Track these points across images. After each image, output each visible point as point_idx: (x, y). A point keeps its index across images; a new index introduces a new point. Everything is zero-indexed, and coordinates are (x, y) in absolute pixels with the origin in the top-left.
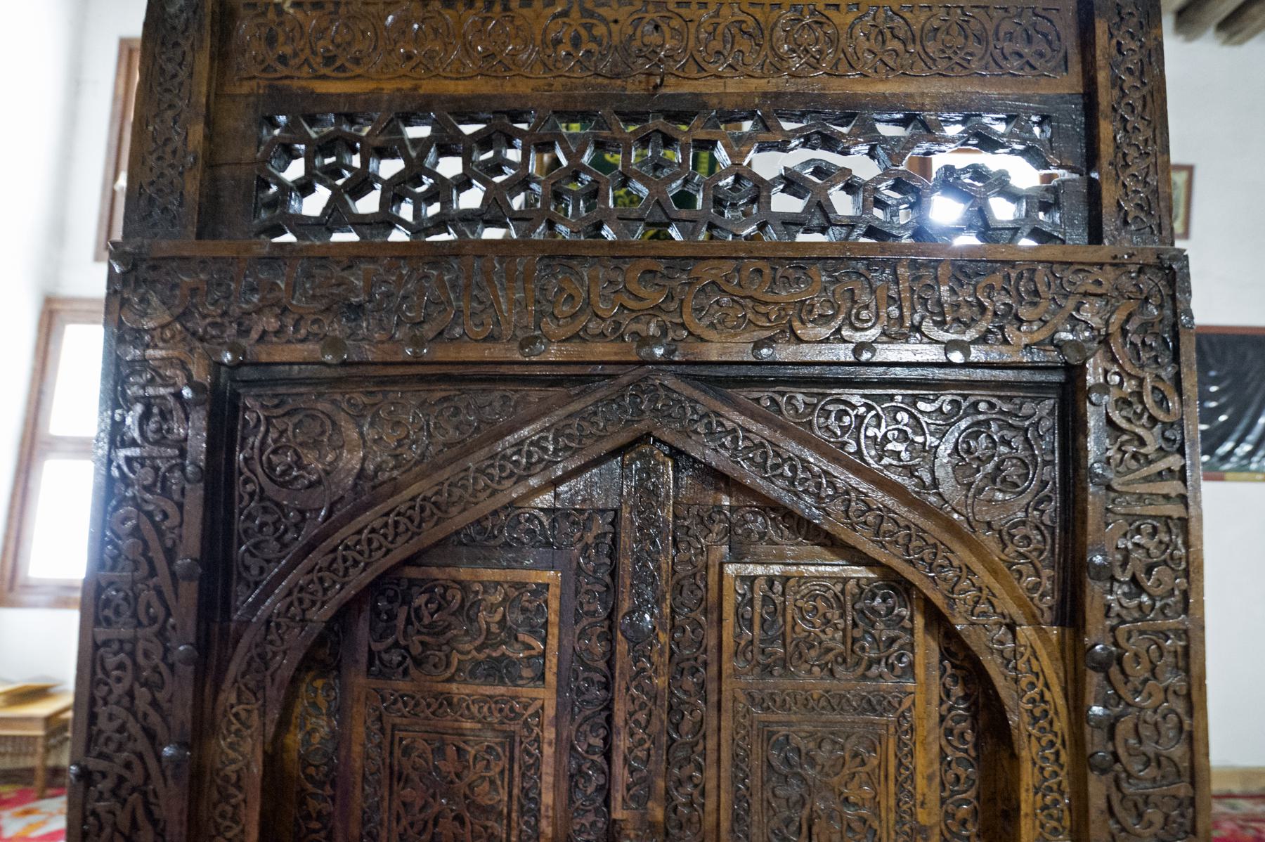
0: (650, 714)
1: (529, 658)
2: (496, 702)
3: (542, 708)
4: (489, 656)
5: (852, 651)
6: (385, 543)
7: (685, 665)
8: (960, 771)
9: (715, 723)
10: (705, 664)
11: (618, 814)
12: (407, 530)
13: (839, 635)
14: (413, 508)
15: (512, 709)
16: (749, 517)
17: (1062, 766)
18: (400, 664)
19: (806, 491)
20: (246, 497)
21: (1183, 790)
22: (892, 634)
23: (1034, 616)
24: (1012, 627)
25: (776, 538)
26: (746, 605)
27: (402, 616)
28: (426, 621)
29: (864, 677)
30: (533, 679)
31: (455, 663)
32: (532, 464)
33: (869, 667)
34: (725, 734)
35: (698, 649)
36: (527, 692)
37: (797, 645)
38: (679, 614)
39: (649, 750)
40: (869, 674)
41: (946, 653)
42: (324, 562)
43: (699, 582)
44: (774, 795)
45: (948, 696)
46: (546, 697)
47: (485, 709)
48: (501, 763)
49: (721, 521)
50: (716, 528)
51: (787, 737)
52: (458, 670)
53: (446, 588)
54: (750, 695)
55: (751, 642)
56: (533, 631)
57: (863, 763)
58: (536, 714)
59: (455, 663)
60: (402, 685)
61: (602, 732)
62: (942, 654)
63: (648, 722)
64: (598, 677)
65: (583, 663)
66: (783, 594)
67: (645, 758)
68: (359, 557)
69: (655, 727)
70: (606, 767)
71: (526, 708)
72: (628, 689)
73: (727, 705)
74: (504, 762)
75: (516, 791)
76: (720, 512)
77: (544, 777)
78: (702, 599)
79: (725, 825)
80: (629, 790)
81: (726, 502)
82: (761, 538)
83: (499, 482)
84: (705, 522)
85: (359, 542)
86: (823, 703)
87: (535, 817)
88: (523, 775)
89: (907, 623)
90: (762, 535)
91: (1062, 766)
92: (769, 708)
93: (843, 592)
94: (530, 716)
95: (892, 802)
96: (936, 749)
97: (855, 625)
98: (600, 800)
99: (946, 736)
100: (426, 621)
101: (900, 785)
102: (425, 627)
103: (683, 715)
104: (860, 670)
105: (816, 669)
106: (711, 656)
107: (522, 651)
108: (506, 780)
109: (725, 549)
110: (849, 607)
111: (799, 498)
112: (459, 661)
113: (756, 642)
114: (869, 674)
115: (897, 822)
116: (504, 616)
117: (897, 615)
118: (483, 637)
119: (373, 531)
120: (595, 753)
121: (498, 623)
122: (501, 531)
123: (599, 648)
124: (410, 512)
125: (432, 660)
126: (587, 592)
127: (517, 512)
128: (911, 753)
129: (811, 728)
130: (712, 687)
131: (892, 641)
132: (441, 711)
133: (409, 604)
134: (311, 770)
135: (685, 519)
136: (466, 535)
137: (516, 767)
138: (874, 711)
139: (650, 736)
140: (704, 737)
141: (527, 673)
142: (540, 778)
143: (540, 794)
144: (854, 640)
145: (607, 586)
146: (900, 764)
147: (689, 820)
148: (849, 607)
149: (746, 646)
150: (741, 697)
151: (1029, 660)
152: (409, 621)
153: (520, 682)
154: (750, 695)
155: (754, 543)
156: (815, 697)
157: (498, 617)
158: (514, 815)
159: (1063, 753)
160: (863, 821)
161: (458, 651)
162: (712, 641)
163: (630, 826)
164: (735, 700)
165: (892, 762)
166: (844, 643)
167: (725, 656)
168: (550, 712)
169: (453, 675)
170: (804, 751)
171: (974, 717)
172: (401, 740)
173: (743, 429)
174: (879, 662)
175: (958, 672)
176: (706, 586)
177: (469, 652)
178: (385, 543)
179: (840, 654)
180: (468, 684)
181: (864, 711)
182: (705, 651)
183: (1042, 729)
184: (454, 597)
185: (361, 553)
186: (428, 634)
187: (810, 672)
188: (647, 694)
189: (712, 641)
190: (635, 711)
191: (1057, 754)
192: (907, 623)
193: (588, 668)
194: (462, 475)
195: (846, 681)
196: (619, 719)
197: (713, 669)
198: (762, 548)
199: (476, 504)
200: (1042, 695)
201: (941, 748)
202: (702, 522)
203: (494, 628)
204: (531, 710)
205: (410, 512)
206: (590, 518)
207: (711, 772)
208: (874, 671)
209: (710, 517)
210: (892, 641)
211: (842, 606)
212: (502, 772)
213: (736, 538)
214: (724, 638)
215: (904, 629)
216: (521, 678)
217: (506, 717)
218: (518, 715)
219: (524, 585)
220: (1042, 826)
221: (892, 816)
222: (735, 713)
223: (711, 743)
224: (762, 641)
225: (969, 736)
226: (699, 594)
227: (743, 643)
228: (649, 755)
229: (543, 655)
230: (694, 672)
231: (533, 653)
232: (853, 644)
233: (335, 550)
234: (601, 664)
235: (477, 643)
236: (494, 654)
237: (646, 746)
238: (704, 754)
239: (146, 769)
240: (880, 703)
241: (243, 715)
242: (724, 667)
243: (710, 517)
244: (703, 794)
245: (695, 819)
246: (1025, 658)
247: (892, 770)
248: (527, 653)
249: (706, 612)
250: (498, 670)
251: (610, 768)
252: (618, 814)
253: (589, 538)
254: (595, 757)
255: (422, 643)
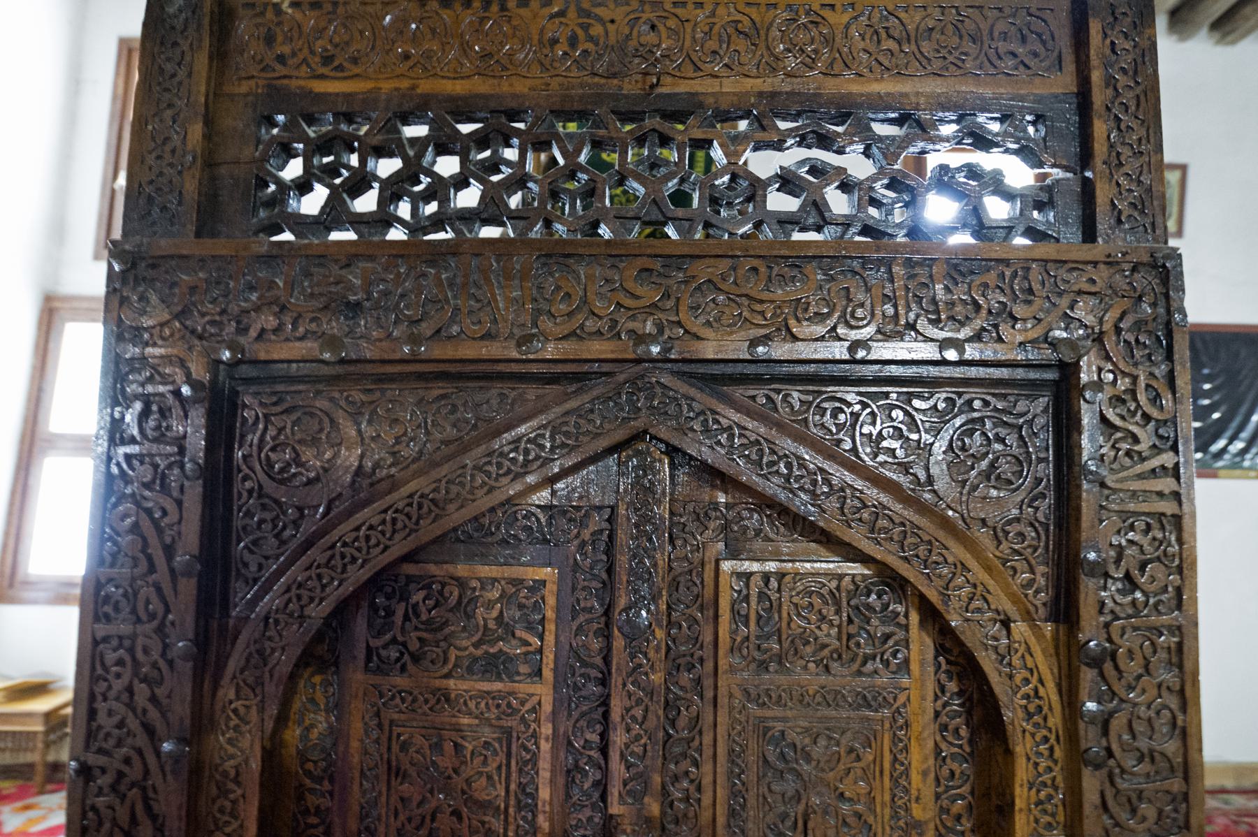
0: (646, 710)
1: (526, 654)
2: (493, 698)
3: (539, 703)
4: (486, 652)
5: (848, 647)
6: (382, 540)
7: (681, 661)
8: (955, 766)
9: (711, 718)
10: (701, 660)
11: (615, 809)
12: (405, 526)
13: (834, 631)
14: (410, 505)
15: (509, 705)
16: (745, 514)
17: (1056, 762)
18: (398, 660)
19: (801, 488)
20: (245, 494)
21: (1176, 785)
22: (887, 630)
23: (1028, 612)
24: (1006, 623)
25: (771, 535)
26: (742, 601)
27: (400, 613)
28: (424, 617)
29: (859, 673)
30: (530, 675)
31: (453, 659)
32: (529, 461)
33: (864, 663)
34: (721, 730)
35: (694, 645)
36: (524, 688)
37: (792, 642)
38: (675, 611)
39: (645, 746)
40: (864, 670)
41: (940, 649)
42: (322, 559)
43: (695, 579)
44: (770, 790)
45: (943, 692)
46: (543, 692)
47: (483, 705)
48: (498, 759)
49: (717, 518)
50: (712, 525)
51: (783, 733)
52: (456, 666)
53: (443, 585)
54: (746, 691)
55: (747, 638)
56: (530, 628)
57: (858, 759)
58: (534, 710)
59: (453, 659)
60: (400, 681)
61: (599, 728)
62: (937, 650)
63: (645, 717)
64: (594, 673)
65: (580, 659)
66: (779, 590)
67: (641, 754)
68: (357, 554)
69: (652, 722)
70: (602, 762)
71: (523, 703)
72: (624, 685)
73: (723, 700)
74: (502, 757)
75: (513, 787)
76: (716, 509)
77: (541, 772)
78: (698, 596)
79: (721, 820)
80: (625, 785)
81: (722, 499)
82: (757, 535)
83: (496, 480)
84: (701, 519)
85: (357, 539)
86: (819, 699)
87: (532, 812)
88: (520, 771)
89: (902, 620)
90: (758, 532)
91: (1056, 762)
92: (765, 704)
93: (838, 588)
94: (527, 712)
95: (887, 797)
96: (931, 744)
97: (850, 621)
98: (596, 795)
99: (941, 732)
100: (424, 617)
101: (895, 781)
102: (423, 623)
103: (679, 711)
104: (855, 666)
105: (812, 665)
106: (707, 652)
107: (519, 647)
108: (503, 775)
109: (721, 545)
110: (844, 603)
111: (795, 495)
112: (457, 657)
113: (752, 638)
114: (864, 670)
115: (892, 817)
116: (501, 612)
117: (892, 612)
118: (480, 633)
119: (371, 528)
120: (591, 749)
121: (495, 619)
122: (498, 528)
123: (596, 644)
124: (407, 509)
125: (430, 656)
126: (584, 589)
127: (514, 509)
128: (906, 749)
129: (806, 724)
130: (708, 682)
131: (887, 637)
132: (438, 707)
133: (407, 600)
134: (310, 766)
135: (681, 516)
136: (463, 532)
137: (513, 763)
138: (869, 706)
139: (646, 731)
140: (700, 733)
141: (524, 669)
142: (537, 773)
143: (537, 789)
144: (850, 637)
145: (604, 583)
146: (895, 759)
147: (685, 815)
148: (844, 603)
149: (742, 642)
150: (737, 693)
151: (1023, 656)
152: (406, 618)
153: (517, 678)
154: (746, 691)
155: (750, 540)
156: (811, 692)
157: (495, 613)
158: (511, 810)
159: (1057, 748)
160: (859, 816)
161: (455, 648)
162: (708, 638)
163: (626, 821)
164: (731, 696)
165: (888, 758)
166: (839, 639)
167: (721, 653)
168: (547, 707)
169: (451, 671)
170: (799, 747)
171: (969, 713)
172: (399, 735)
173: (739, 426)
174: (874, 658)
175: (953, 668)
176: (702, 582)
177: (466, 648)
178: (382, 540)
179: (836, 650)
180: (465, 680)
181: (859, 707)
182: (702, 647)
183: (1036, 725)
184: (451, 593)
185: (359, 550)
186: (426, 630)
187: (805, 668)
188: (643, 690)
189: (708, 638)
190: (632, 707)
191: (1051, 749)
192: (902, 620)
193: (585, 664)
194: (459, 472)
195: (842, 677)
196: (616, 715)
197: (709, 665)
198: (758, 544)
199: (474, 501)
200: (1036, 691)
201: (936, 743)
202: (698, 519)
203: (492, 625)
204: (528, 706)
205: (407, 509)
206: (587, 515)
207: (707, 768)
208: (869, 667)
209: (706, 514)
210: (887, 637)
211: (837, 603)
212: (499, 767)
213: (732, 535)
214: (720, 634)
215: (899, 625)
216: (518, 674)
217: (503, 713)
218: (515, 711)
219: (522, 581)
220: (1037, 821)
221: (887, 811)
222: (731, 708)
223: (707, 739)
224: (758, 637)
225: (964, 732)
226: (695, 590)
227: (739, 639)
228: (645, 751)
229: (540, 651)
230: (690, 668)
231: (530, 649)
232: (848, 640)
233: (333, 546)
234: (598, 660)
235: (475, 639)
236: (492, 651)
237: (643, 741)
238: (700, 750)
239: (145, 764)
240: (875, 699)
241: (242, 711)
242: (720, 663)
243: (706, 514)
244: (699, 789)
245: (691, 814)
246: (1019, 654)
247: (887, 766)
248: (524, 649)
249: (702, 609)
250: (496, 666)
251: (606, 763)
252: (615, 809)
253: (586, 535)
254: (592, 753)
255: (420, 639)
